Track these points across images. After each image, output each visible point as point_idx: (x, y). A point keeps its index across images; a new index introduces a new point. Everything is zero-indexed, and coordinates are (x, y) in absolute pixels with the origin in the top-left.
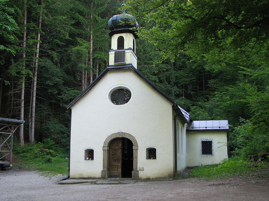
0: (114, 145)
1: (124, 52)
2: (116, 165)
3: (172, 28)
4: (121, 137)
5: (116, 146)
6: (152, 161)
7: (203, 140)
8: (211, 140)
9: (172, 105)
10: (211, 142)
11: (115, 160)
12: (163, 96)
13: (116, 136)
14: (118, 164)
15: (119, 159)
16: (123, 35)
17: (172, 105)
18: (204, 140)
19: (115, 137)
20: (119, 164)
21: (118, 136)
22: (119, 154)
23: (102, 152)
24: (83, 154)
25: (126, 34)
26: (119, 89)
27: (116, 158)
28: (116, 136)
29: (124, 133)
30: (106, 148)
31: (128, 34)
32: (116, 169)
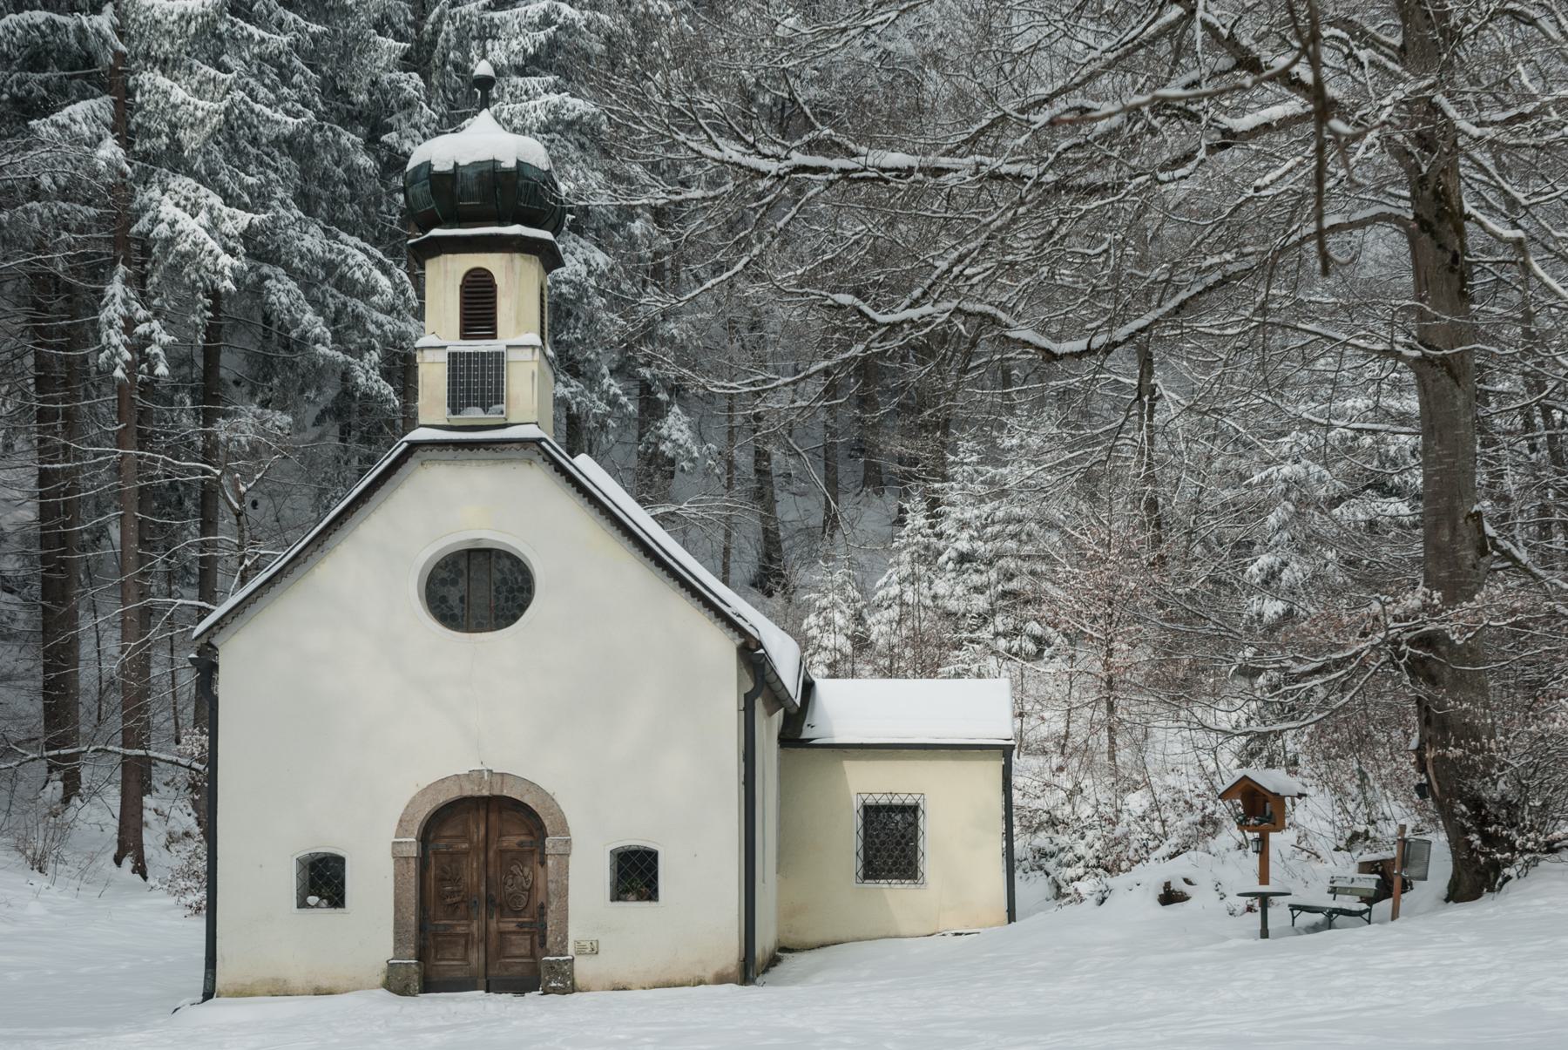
0: (448, 833)
1: (497, 362)
2: (460, 930)
3: (1371, 137)
4: (485, 793)
5: (457, 837)
6: (634, 910)
7: (871, 801)
8: (917, 797)
9: (739, 641)
10: (913, 810)
11: (455, 906)
12: (645, 556)
13: (461, 788)
14: (468, 926)
15: (476, 899)
16: (492, 262)
17: (739, 641)
18: (877, 797)
19: (454, 793)
20: (475, 925)
21: (470, 790)
22: (475, 879)
23: (388, 867)
24: (288, 881)
25: (506, 256)
26: (469, 551)
27: (457, 899)
28: (461, 788)
29: (502, 774)
30: (412, 849)
31: (517, 256)
32: (460, 951)
